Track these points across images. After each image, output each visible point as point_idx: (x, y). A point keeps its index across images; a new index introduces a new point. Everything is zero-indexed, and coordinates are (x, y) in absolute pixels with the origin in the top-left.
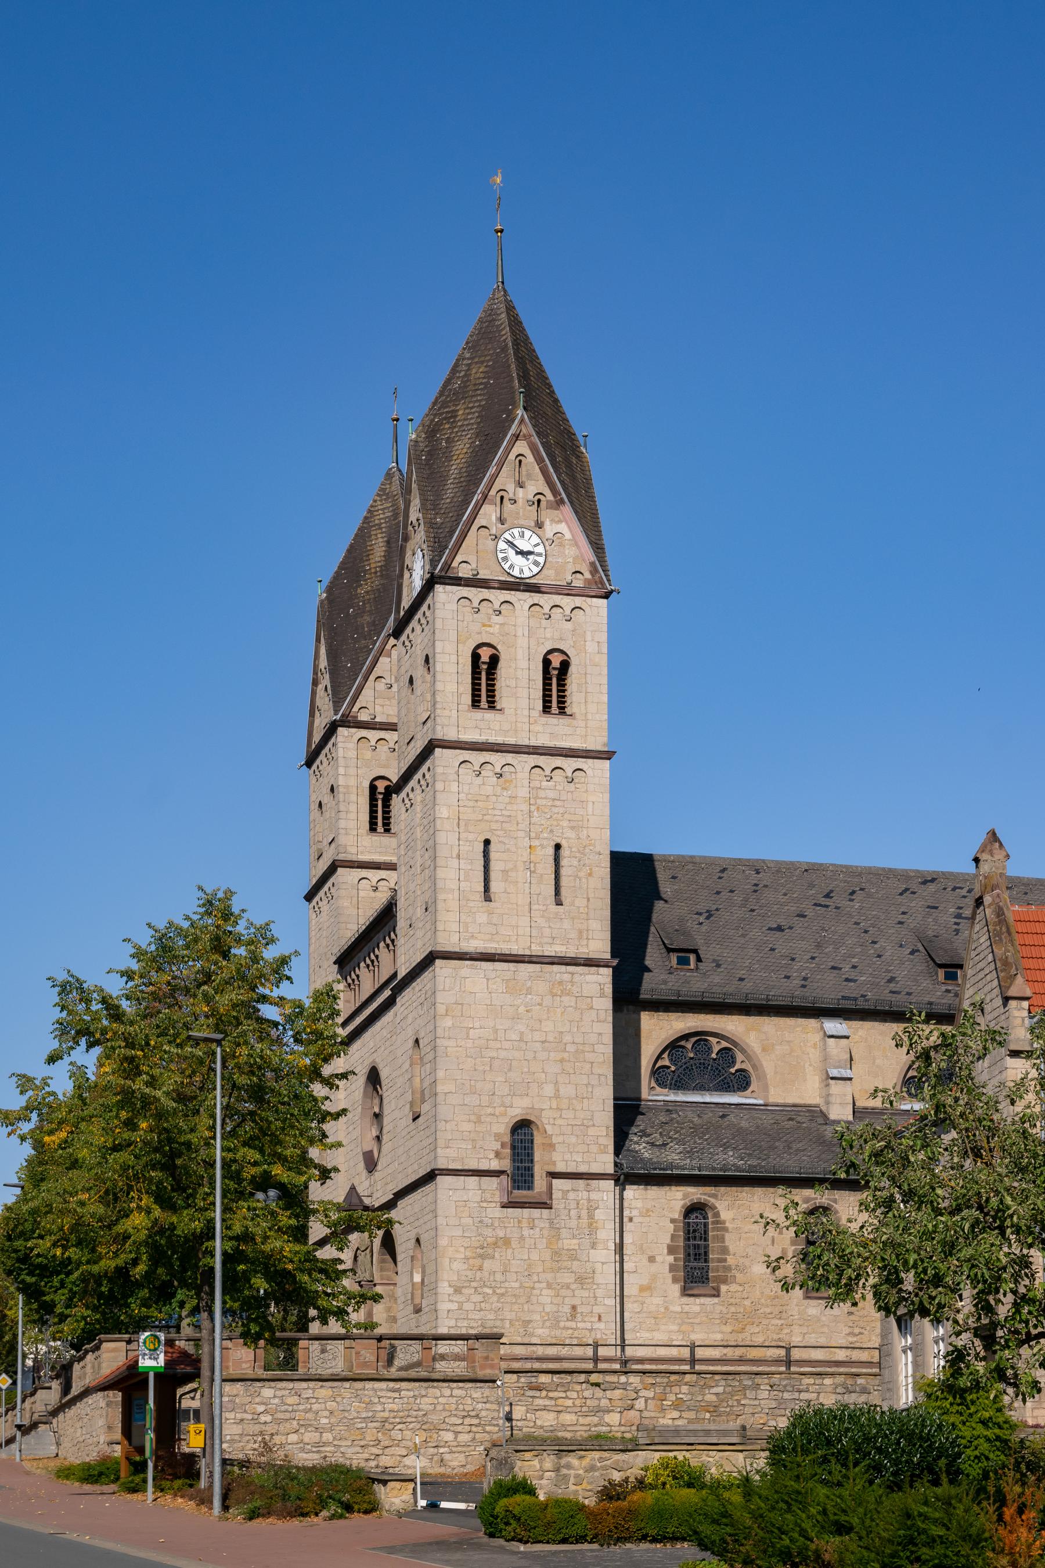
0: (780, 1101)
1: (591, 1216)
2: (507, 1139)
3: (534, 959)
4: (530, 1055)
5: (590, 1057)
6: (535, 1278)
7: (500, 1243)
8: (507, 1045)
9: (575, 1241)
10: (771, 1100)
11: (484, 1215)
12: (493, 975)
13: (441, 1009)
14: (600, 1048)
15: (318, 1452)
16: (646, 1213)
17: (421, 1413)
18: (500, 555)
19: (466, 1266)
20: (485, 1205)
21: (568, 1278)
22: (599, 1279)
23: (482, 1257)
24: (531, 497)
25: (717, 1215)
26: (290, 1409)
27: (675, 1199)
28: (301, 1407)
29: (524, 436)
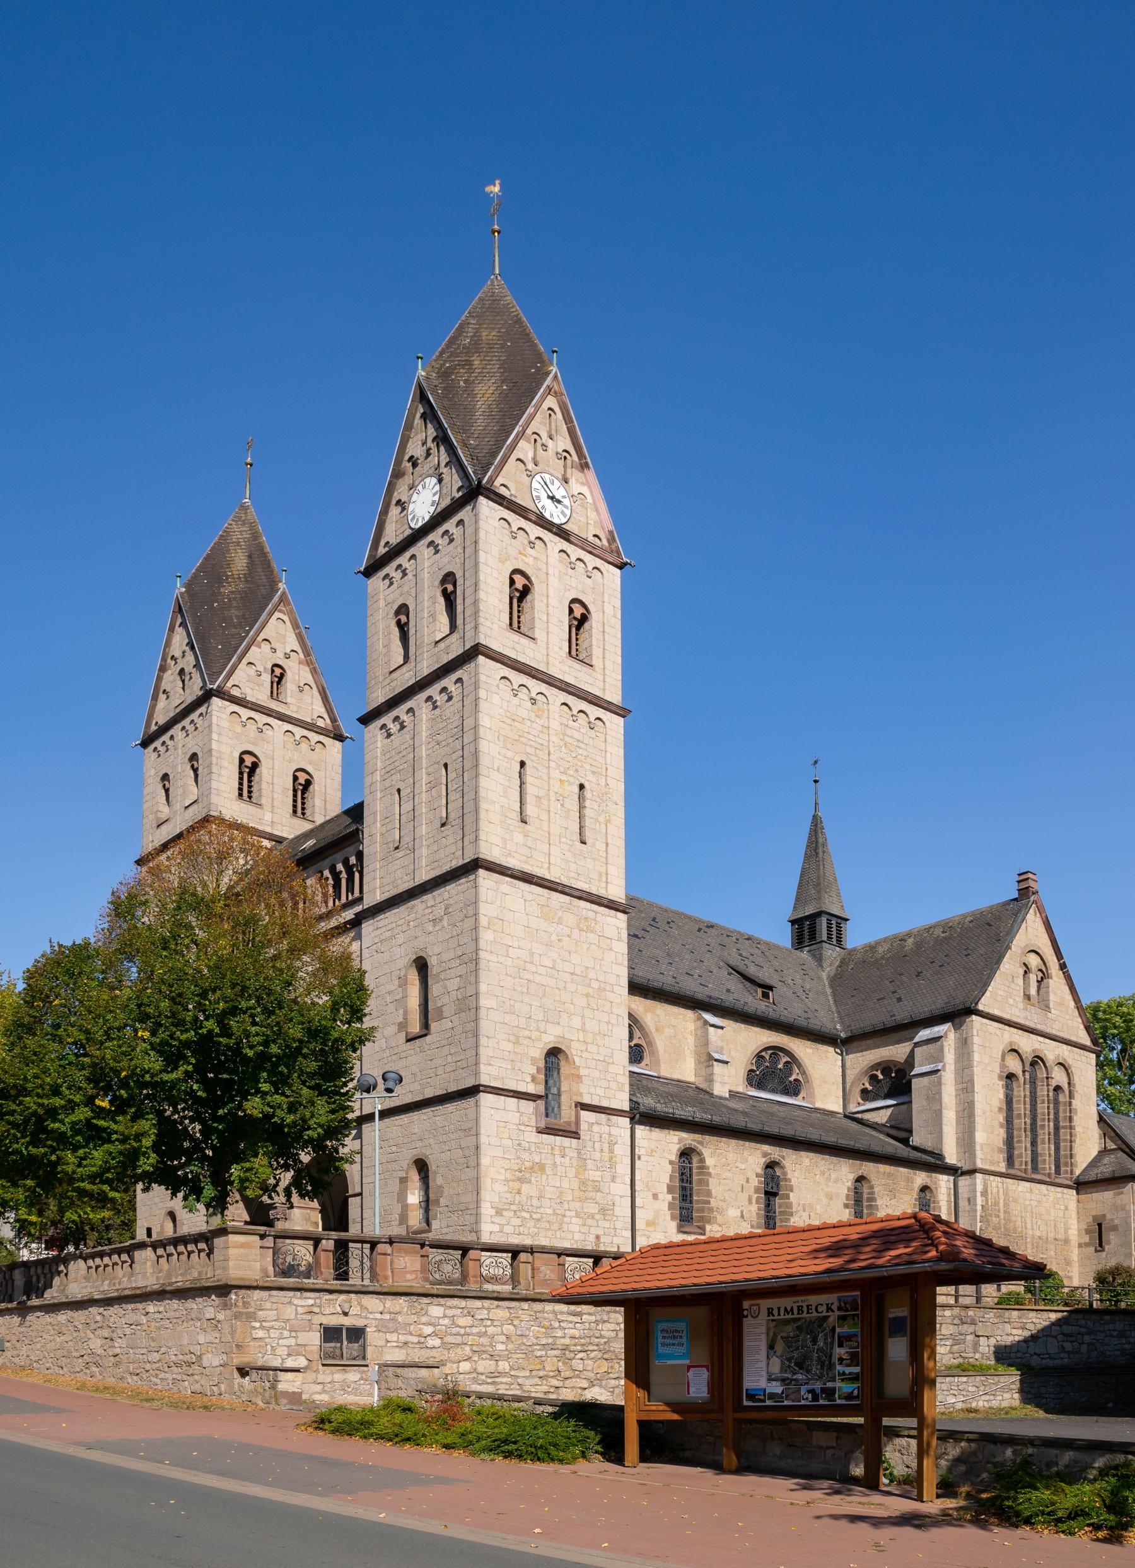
0: (669, 1076)
1: (611, 1151)
2: (542, 1064)
3: (567, 890)
4: (561, 985)
5: (610, 995)
6: (566, 1206)
7: (536, 1168)
8: (541, 970)
9: (599, 1173)
10: (662, 1074)
11: (521, 1138)
12: (529, 897)
13: (483, 921)
14: (617, 989)
15: (492, 1383)
16: (651, 1153)
17: (603, 1341)
18: (535, 494)
19: (506, 1189)
20: (522, 1128)
21: (593, 1209)
22: (618, 1211)
23: (521, 1180)
24: (560, 450)
25: (702, 1161)
26: (462, 1331)
27: (672, 1141)
28: (475, 1330)
29: (555, 392)
